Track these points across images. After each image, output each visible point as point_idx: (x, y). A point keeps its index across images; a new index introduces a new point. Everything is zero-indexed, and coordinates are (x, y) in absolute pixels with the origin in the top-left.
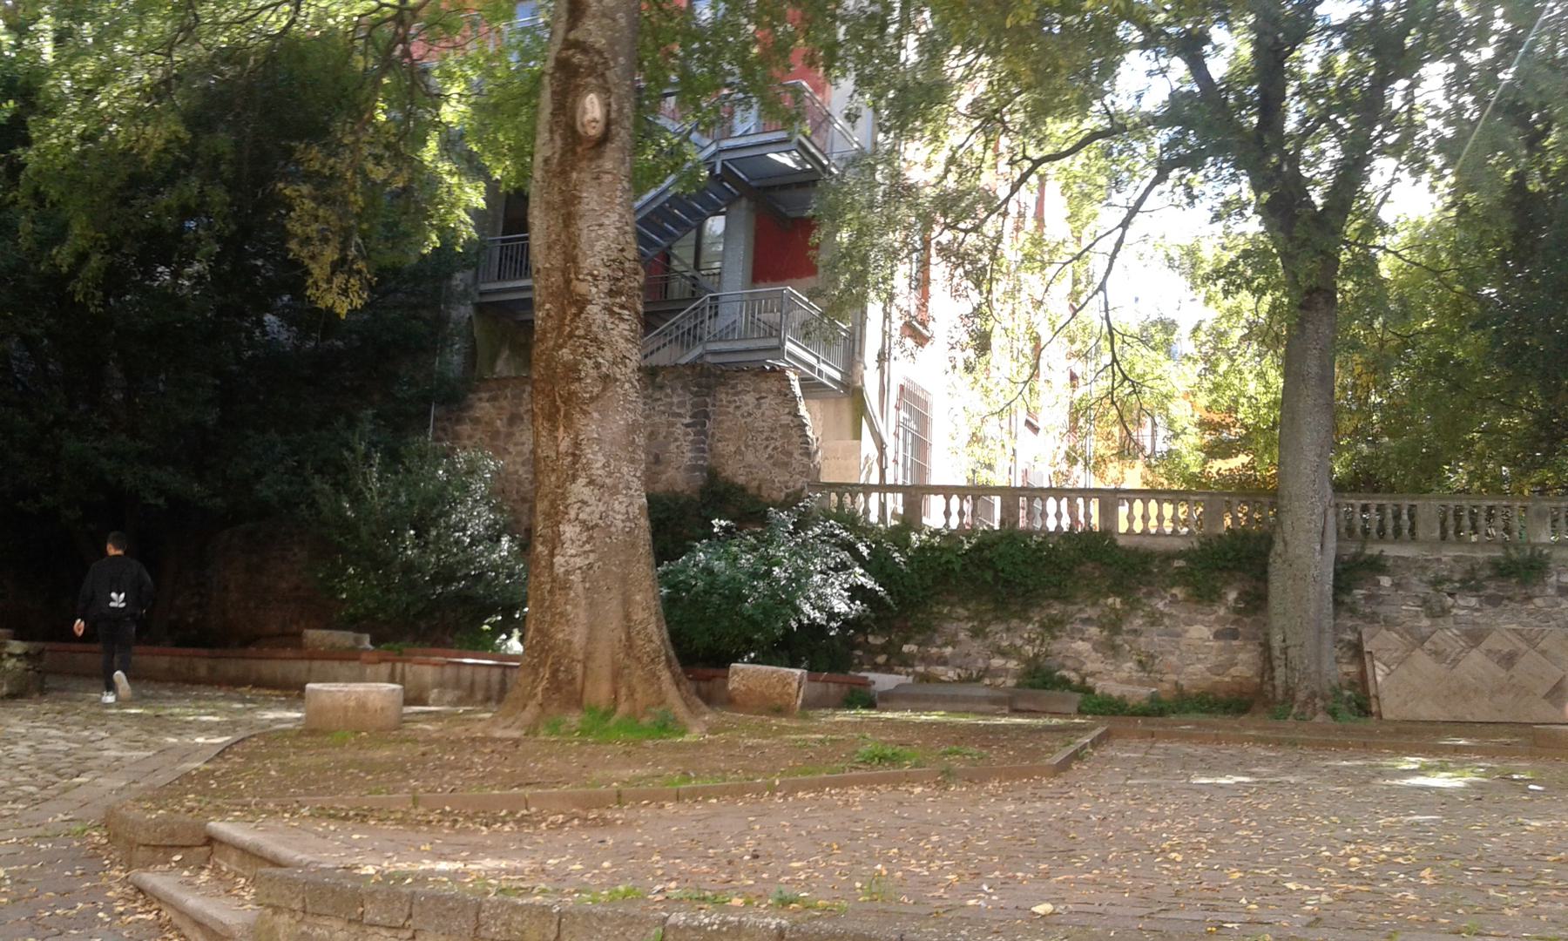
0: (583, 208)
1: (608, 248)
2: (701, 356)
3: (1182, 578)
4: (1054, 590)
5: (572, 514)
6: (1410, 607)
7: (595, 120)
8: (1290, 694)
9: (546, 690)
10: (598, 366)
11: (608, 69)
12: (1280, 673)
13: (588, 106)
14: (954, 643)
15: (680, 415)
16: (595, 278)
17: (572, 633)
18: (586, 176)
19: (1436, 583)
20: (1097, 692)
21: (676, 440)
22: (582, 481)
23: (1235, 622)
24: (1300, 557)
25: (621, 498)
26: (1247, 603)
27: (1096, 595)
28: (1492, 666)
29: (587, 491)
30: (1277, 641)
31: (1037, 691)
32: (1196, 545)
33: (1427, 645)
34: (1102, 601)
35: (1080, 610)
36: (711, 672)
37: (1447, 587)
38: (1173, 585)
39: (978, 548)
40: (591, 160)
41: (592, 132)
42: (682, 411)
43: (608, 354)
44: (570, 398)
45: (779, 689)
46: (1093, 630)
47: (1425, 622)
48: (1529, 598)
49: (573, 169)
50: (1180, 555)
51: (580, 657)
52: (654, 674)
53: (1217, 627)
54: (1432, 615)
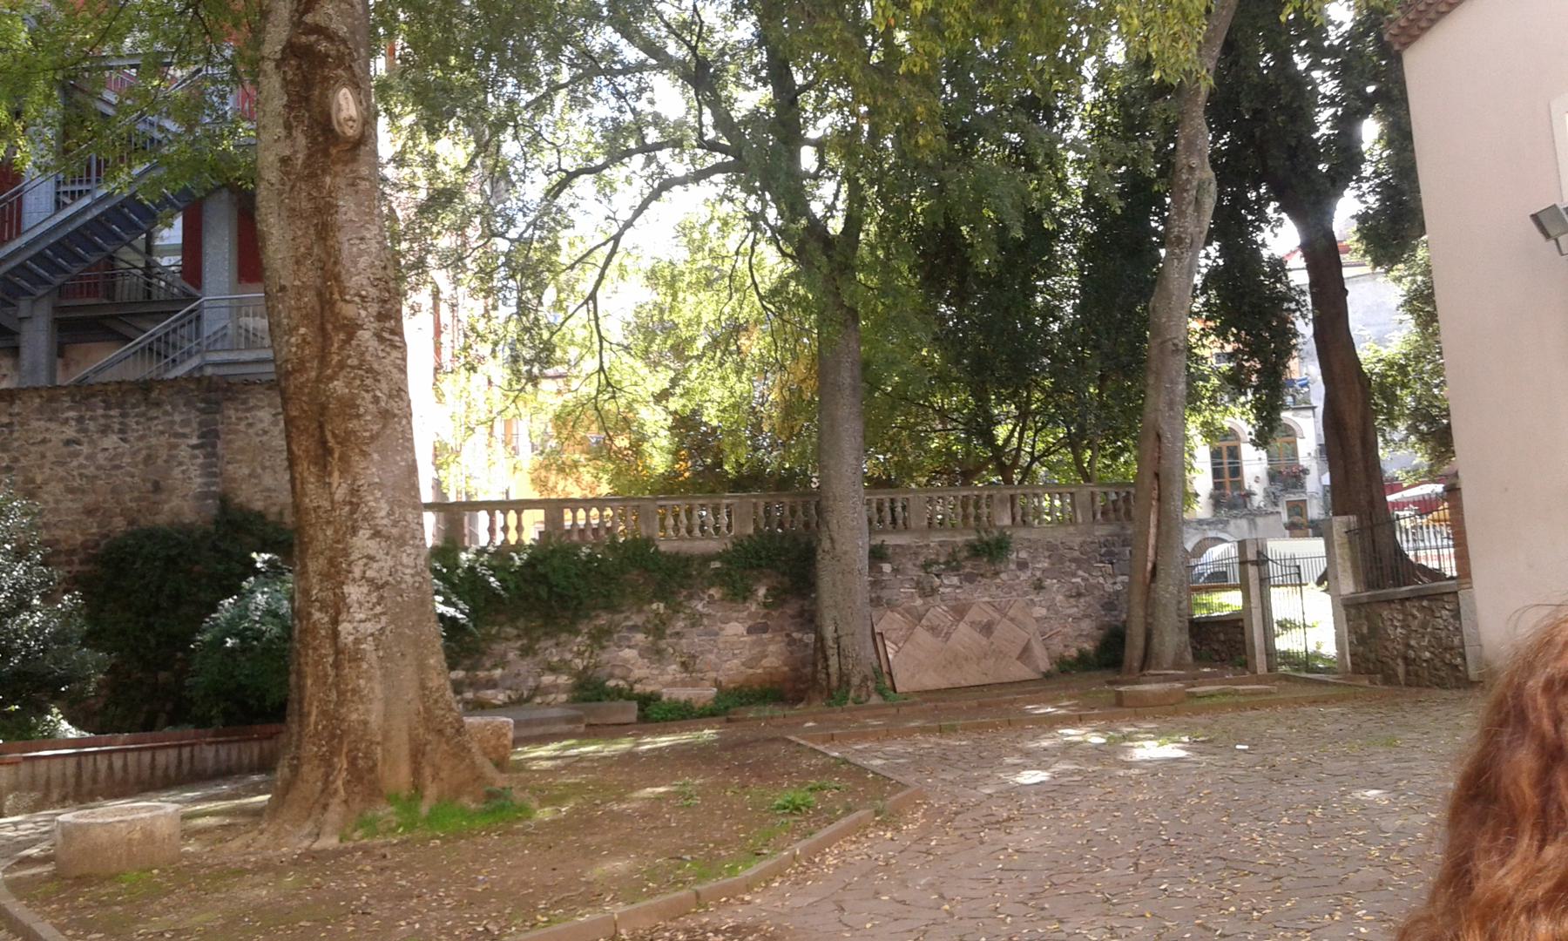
0: (341, 218)
1: (372, 265)
2: (200, 368)
3: (719, 578)
4: (601, 600)
5: (357, 572)
6: (908, 589)
7: (351, 119)
8: (844, 680)
9: (347, 783)
10: (376, 400)
11: (354, 60)
12: (833, 661)
13: (343, 102)
14: (502, 663)
15: (184, 436)
16: (363, 298)
17: (368, 711)
18: (341, 182)
19: (926, 566)
20: (665, 698)
21: (181, 464)
22: (364, 533)
23: (765, 616)
24: (845, 553)
25: (409, 550)
26: (775, 597)
27: (641, 602)
28: (976, 635)
29: (373, 544)
30: (829, 632)
31: (594, 704)
32: (730, 546)
33: (924, 622)
34: (646, 608)
35: (627, 618)
36: (273, 728)
37: (934, 569)
38: (712, 585)
39: (530, 564)
40: (346, 163)
41: (350, 132)
42: (187, 430)
43: (384, 386)
44: (346, 439)
45: (493, 742)
46: (640, 637)
47: (919, 602)
48: (997, 574)
49: (324, 171)
50: (718, 556)
51: (379, 739)
52: (464, 748)
53: (750, 623)
54: (924, 595)
